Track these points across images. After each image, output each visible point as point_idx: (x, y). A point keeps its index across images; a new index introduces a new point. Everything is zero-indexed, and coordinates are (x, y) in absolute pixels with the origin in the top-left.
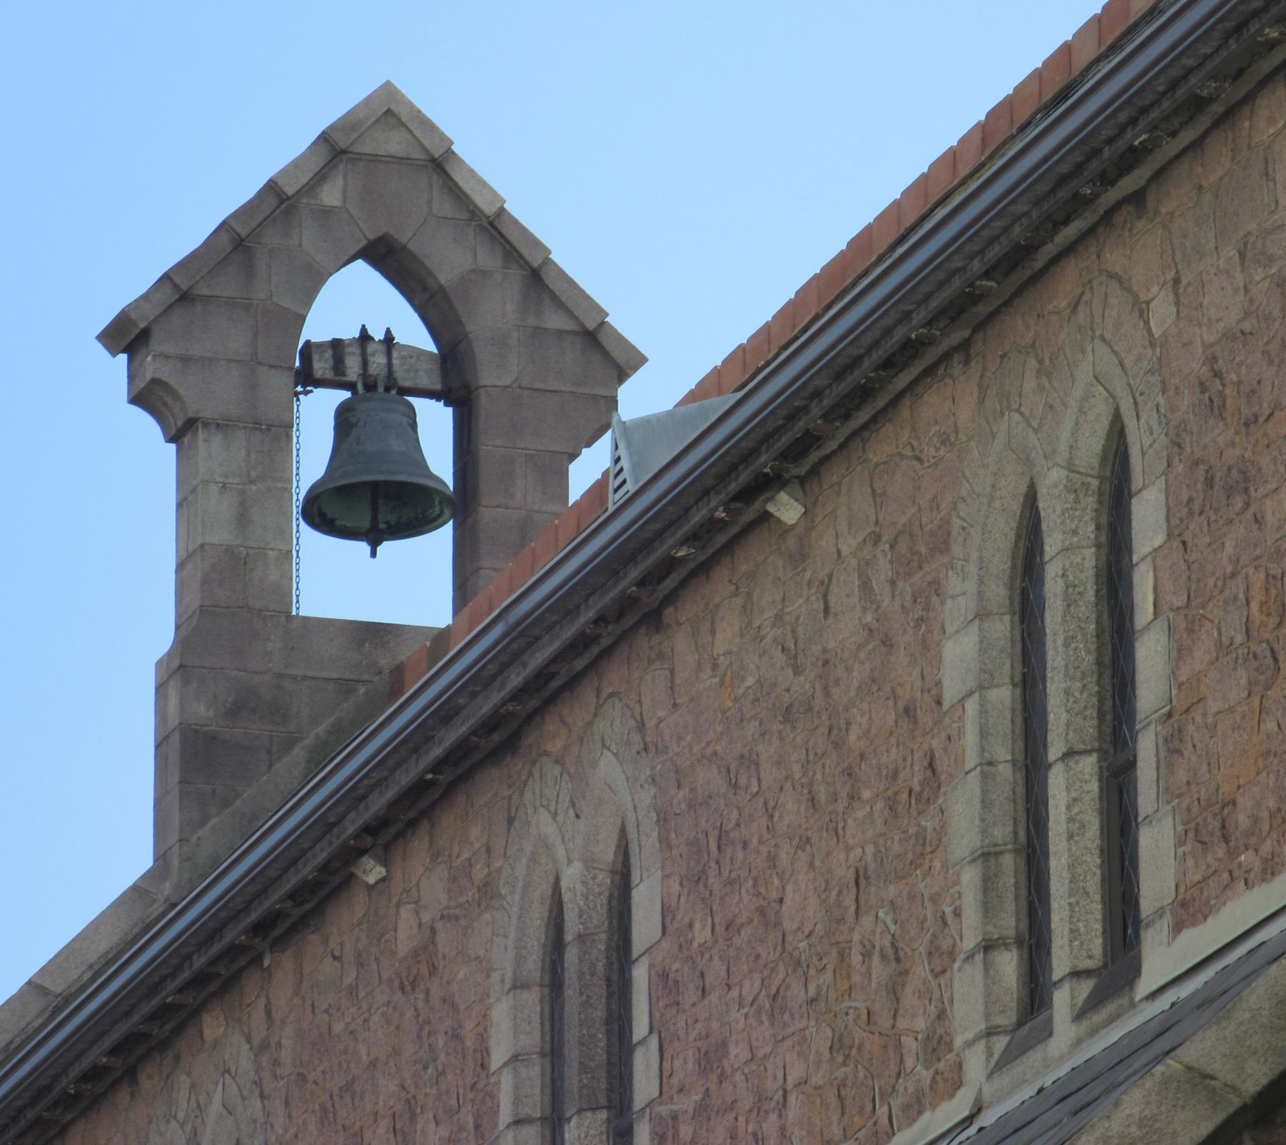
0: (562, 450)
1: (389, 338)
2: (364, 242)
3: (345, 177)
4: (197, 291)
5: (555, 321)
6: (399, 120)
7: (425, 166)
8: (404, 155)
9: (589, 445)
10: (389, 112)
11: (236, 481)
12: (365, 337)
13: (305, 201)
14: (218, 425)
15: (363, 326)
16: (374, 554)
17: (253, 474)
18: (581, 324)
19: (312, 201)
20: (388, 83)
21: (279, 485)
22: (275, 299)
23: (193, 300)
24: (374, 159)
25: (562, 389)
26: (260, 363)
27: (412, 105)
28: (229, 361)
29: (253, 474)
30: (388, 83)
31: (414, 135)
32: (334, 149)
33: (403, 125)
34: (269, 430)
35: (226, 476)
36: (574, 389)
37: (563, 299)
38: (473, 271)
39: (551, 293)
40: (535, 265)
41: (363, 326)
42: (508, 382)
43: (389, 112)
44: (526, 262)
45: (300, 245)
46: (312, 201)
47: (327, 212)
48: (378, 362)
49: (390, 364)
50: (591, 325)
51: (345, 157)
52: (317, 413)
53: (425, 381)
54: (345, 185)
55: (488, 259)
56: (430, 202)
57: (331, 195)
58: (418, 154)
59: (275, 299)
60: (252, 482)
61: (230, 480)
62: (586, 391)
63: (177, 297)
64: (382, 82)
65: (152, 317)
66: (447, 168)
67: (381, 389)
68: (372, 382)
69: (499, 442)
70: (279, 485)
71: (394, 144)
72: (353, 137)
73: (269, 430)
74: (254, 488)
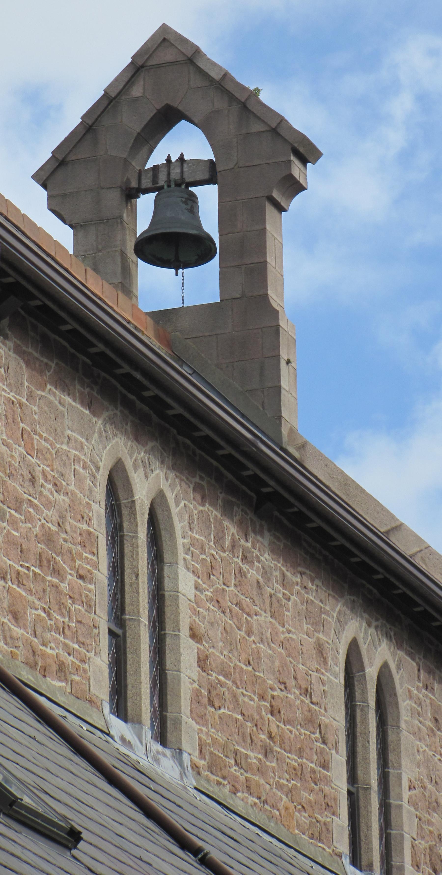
0: (262, 195)
1: (181, 158)
2: (155, 111)
3: (144, 80)
4: (69, 159)
5: (256, 127)
6: (170, 42)
7: (186, 63)
8: (175, 60)
9: (3, 197)
10: (164, 40)
11: (91, 252)
12: (169, 159)
13: (123, 98)
14: (81, 225)
15: (169, 155)
16: (177, 274)
17: (100, 247)
18: (269, 126)
19: (127, 97)
20: (164, 24)
21: (114, 249)
22: (109, 153)
23: (67, 164)
24: (159, 66)
25: (262, 163)
26: (102, 188)
27: (176, 33)
28: (86, 191)
29: (100, 247)
30: (164, 24)
31: (177, 48)
32: (140, 67)
33: (173, 45)
34: (107, 222)
35: (86, 251)
36: (268, 161)
37: (258, 115)
38: (212, 112)
39: (255, 115)
40: (243, 100)
41: (169, 155)
42: (232, 166)
43: (164, 40)
44: (240, 101)
45: (121, 122)
46: (127, 97)
47: (136, 100)
48: (176, 173)
49: (182, 172)
50: (274, 125)
51: (143, 69)
52: (145, 205)
53: (200, 177)
54: (144, 84)
55: (220, 103)
56: (189, 81)
57: (137, 91)
58: (181, 58)
59: (109, 153)
60: (100, 251)
61: (88, 253)
62: (274, 161)
63: (57, 164)
64: (160, 24)
65: (45, 178)
66: (195, 61)
67: (166, 187)
68: (176, 184)
69: (228, 199)
70: (114, 249)
71: (168, 56)
72: (146, 57)
73: (107, 222)
74: (100, 254)
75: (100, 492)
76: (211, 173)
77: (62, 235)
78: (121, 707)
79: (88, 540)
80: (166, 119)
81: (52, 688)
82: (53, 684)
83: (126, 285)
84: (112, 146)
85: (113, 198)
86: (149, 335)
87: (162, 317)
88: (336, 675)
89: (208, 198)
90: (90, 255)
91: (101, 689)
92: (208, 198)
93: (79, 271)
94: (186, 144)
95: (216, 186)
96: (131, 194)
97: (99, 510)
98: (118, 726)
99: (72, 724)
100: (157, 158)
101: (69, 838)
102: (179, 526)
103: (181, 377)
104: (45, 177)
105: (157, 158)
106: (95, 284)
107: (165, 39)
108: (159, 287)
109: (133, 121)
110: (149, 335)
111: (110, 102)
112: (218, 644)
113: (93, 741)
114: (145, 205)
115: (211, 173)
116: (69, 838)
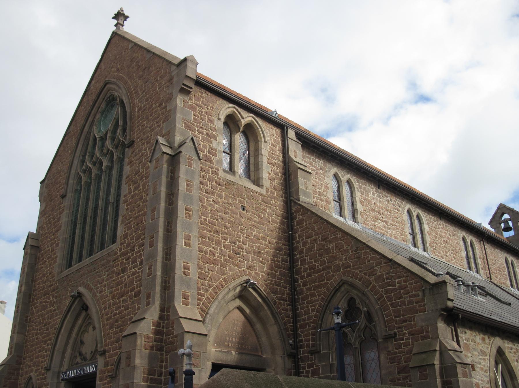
32: (498, 209)
52: (503, 225)
68: (506, 221)
75: (504, 261)
76: (510, 220)
77: (493, 230)
78: (512, 287)
79: (504, 267)
80: (503, 214)
81: (503, 286)
82: (503, 285)
83: (502, 235)
84: (497, 219)
85: (498, 225)
86: (506, 240)
87: (507, 238)
88: (491, 259)
89: (510, 223)
90: (496, 232)
91: (509, 285)
92: (510, 223)
93: (496, 234)
94: (506, 216)
95: (35, 232)
96: (500, 224)
97: (505, 263)
98: (512, 289)
99: (506, 290)
100: (503, 219)
101: (509, 304)
102: (515, 263)
103: (511, 245)
104: (489, 224)
105: (503, 219)
106: (498, 235)
107: (501, 205)
108: (506, 235)
109: (499, 215)
110: (506, 240)
111: (496, 213)
112: (214, 144)
113: (509, 291)
114: (503, 225)
115: (510, 220)
116: (509, 304)
